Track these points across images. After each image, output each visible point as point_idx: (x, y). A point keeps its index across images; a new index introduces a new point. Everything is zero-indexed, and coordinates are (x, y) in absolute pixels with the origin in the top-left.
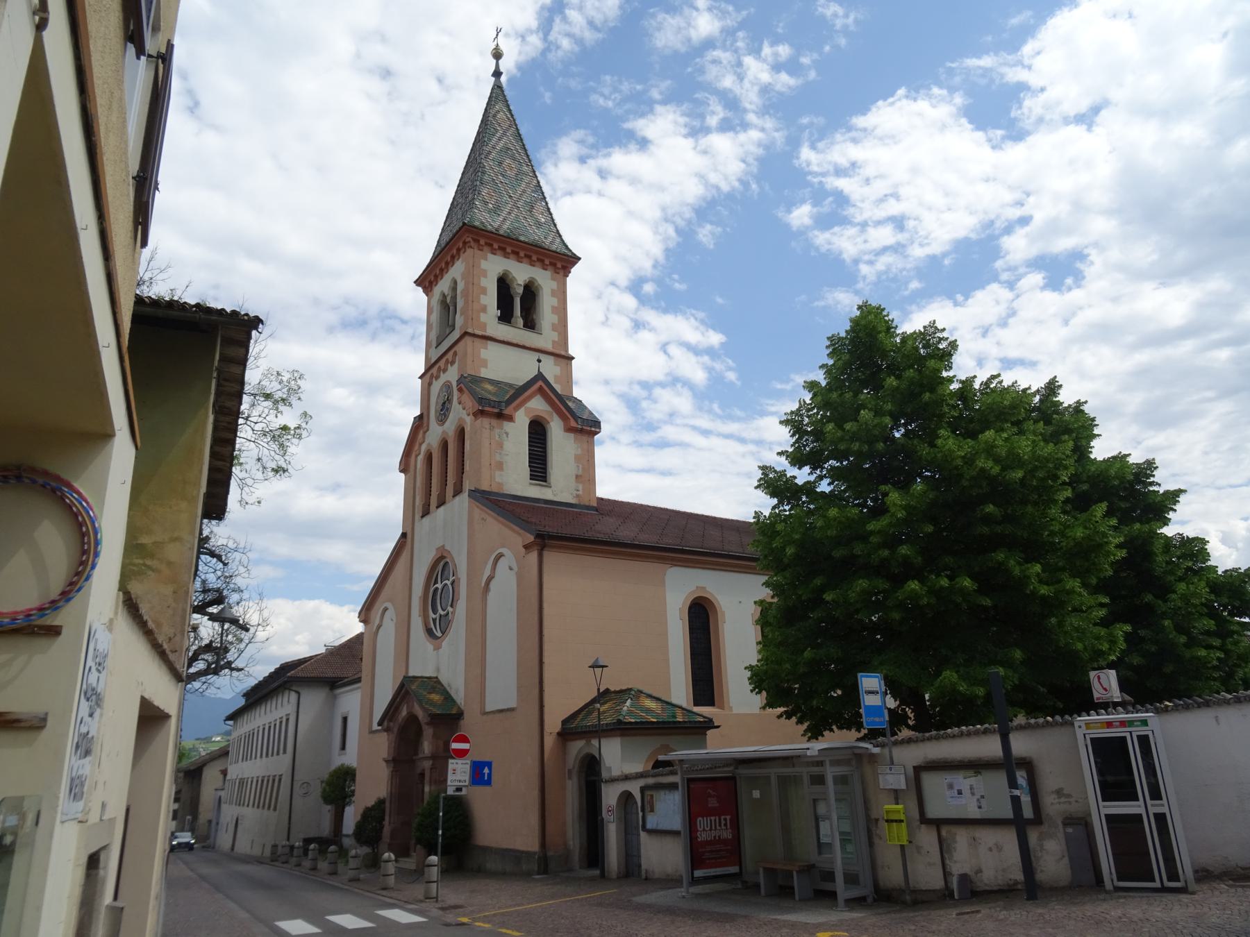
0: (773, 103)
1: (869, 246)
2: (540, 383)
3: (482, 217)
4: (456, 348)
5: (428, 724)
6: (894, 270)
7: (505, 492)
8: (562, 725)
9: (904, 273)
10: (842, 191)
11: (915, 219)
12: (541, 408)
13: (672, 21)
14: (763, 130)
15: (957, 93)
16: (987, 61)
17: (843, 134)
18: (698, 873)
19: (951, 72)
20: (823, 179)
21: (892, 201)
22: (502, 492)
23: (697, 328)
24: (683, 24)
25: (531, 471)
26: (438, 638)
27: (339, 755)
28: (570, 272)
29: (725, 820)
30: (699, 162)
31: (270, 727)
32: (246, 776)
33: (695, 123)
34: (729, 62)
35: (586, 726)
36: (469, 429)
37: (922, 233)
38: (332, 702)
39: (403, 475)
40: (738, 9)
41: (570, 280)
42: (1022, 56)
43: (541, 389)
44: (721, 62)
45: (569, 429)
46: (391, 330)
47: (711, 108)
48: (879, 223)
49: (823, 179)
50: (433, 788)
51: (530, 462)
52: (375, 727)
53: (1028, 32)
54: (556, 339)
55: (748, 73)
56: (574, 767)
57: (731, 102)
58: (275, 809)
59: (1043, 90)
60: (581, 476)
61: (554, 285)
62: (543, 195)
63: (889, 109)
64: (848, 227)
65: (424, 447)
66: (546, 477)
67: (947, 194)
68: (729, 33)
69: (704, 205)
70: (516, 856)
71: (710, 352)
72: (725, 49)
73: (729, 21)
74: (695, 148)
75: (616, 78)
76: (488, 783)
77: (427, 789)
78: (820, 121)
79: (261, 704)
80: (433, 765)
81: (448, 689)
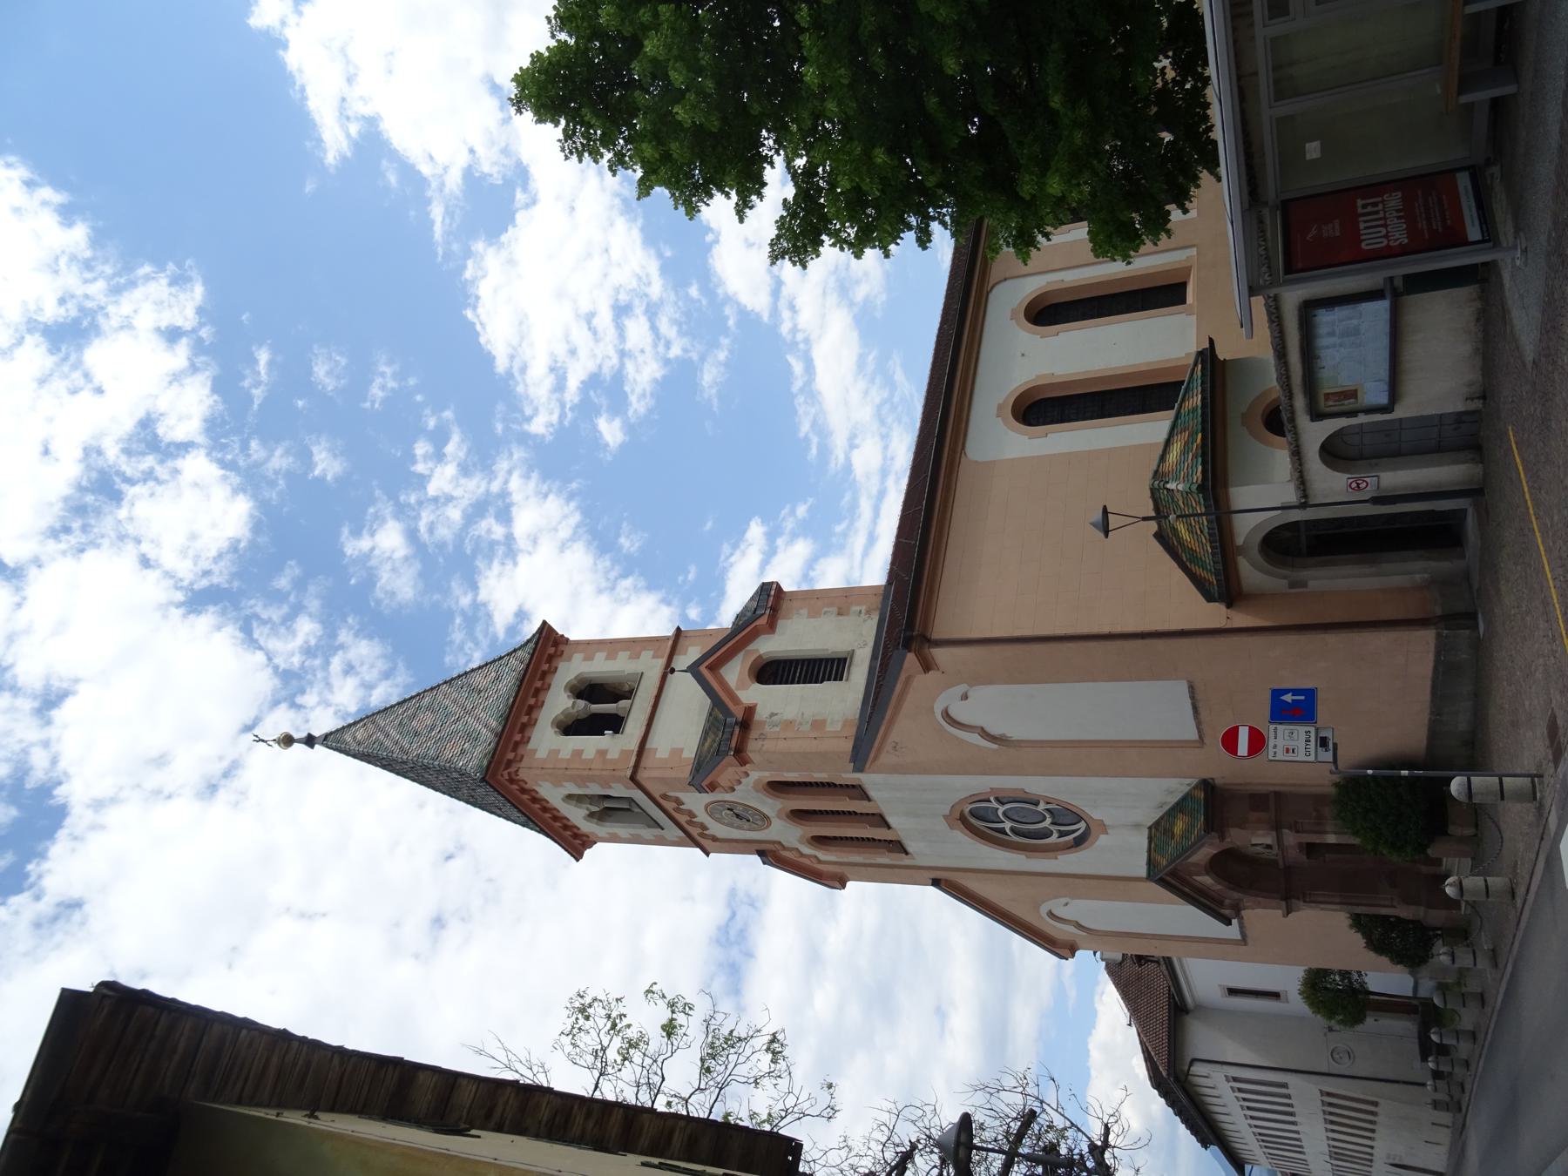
0: (480, 459)
1: (648, 349)
2: (703, 669)
3: (473, 758)
4: (657, 796)
5: (1222, 838)
6: (677, 316)
7: (857, 716)
8: (1215, 601)
9: (680, 303)
10: (582, 382)
11: (618, 293)
12: (738, 668)
13: (384, 576)
14: (510, 472)
15: (473, 248)
16: (437, 212)
17: (517, 383)
18: (1474, 233)
19: (448, 255)
20: (568, 406)
21: (595, 321)
22: (857, 721)
23: (743, 554)
24: (388, 567)
25: (829, 680)
26: (1088, 828)
27: (1288, 1002)
28: (562, 636)
29: (1364, 206)
30: (546, 548)
31: (1249, 1108)
32: (1326, 1150)
33: (500, 552)
34: (433, 512)
35: (1213, 554)
36: (767, 774)
37: (634, 284)
38: (1202, 1010)
39: (849, 884)
40: (372, 501)
41: (573, 635)
42: (433, 176)
43: (712, 668)
44: (432, 523)
45: (771, 627)
46: (743, 934)
47: (483, 533)
48: (622, 336)
49: (568, 406)
50: (1328, 828)
51: (816, 682)
52: (1233, 931)
53: (408, 172)
54: (651, 653)
55: (446, 490)
56: (1285, 577)
57: (478, 509)
58: (1376, 1104)
59: (472, 151)
60: (839, 608)
61: (578, 657)
62: (462, 675)
63: (489, 329)
64: (625, 372)
65: (806, 850)
66: (839, 659)
67: (589, 255)
68: (401, 512)
69: (596, 543)
70: (1444, 672)
71: (771, 537)
72: (417, 518)
73: (387, 511)
74: (530, 553)
75: (448, 649)
76: (1310, 694)
77: (1331, 839)
78: (500, 407)
79: (1215, 1121)
80: (1290, 828)
81: (1167, 808)
